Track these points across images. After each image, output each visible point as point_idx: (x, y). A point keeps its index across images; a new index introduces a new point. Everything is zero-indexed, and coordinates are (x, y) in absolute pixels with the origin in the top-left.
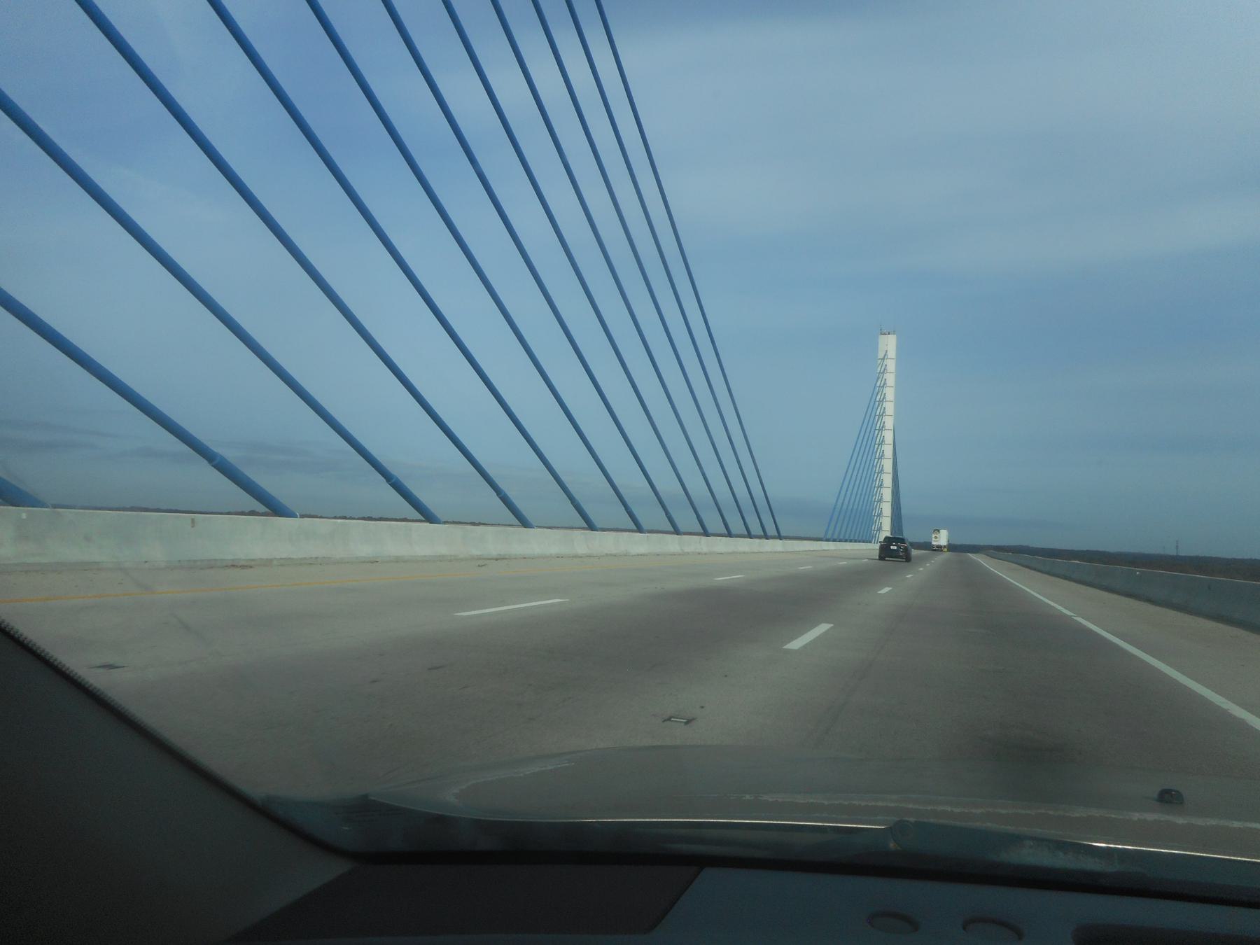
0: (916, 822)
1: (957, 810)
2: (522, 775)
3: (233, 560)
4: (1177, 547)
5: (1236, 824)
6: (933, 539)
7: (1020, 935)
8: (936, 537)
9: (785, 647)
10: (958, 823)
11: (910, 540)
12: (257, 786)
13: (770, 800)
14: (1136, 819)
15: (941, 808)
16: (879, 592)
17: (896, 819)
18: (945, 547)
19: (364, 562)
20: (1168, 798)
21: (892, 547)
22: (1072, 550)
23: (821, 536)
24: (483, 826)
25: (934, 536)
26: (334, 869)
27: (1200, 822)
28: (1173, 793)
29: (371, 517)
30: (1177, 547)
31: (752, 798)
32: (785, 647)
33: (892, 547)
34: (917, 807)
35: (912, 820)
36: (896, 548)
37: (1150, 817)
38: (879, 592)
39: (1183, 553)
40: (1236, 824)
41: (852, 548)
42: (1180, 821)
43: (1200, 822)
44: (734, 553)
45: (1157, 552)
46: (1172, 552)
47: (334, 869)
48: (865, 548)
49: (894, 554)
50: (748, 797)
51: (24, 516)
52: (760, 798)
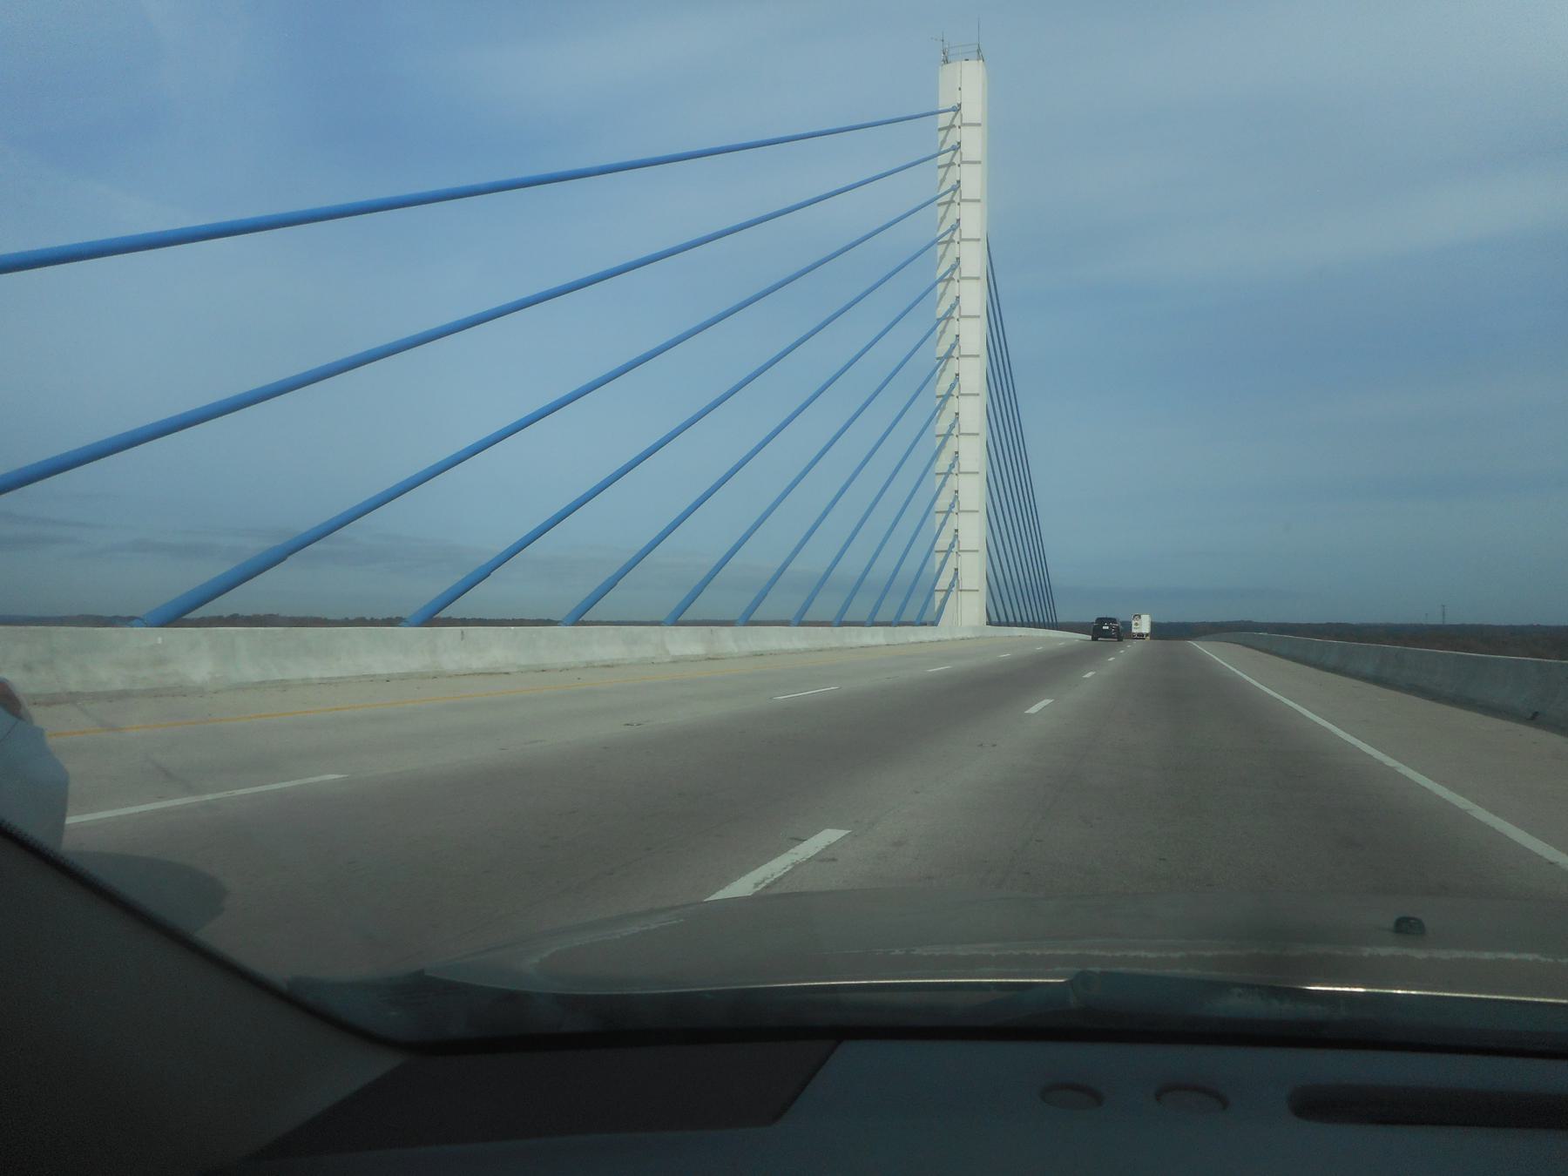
0: (1102, 972)
1: (1150, 955)
2: (618, 937)
3: (389, 674)
4: (1444, 614)
5: (1487, 955)
6: (1133, 626)
7: (1224, 1103)
8: (1136, 624)
9: (842, 833)
10: (1153, 971)
11: (1121, 620)
12: (279, 967)
13: (925, 954)
14: (1366, 954)
15: (1132, 954)
16: (1027, 712)
17: (1079, 970)
18: (1147, 635)
19: (756, 655)
20: (1407, 927)
21: (1104, 628)
22: (1184, 623)
23: (865, 618)
24: (569, 1003)
25: (1133, 622)
26: (383, 1063)
27: (1443, 955)
28: (1412, 921)
29: (276, 616)
30: (1444, 614)
31: (904, 952)
32: (842, 833)
33: (1104, 628)
34: (1103, 953)
35: (1097, 969)
36: (1108, 628)
37: (1384, 952)
38: (1027, 712)
39: (1448, 622)
40: (1487, 955)
41: (931, 639)
42: (1420, 955)
43: (1443, 955)
44: (839, 649)
45: (1415, 621)
46: (1435, 620)
47: (383, 1063)
48: (835, 644)
49: (1106, 634)
50: (897, 952)
51: (160, 640)
52: (912, 953)
